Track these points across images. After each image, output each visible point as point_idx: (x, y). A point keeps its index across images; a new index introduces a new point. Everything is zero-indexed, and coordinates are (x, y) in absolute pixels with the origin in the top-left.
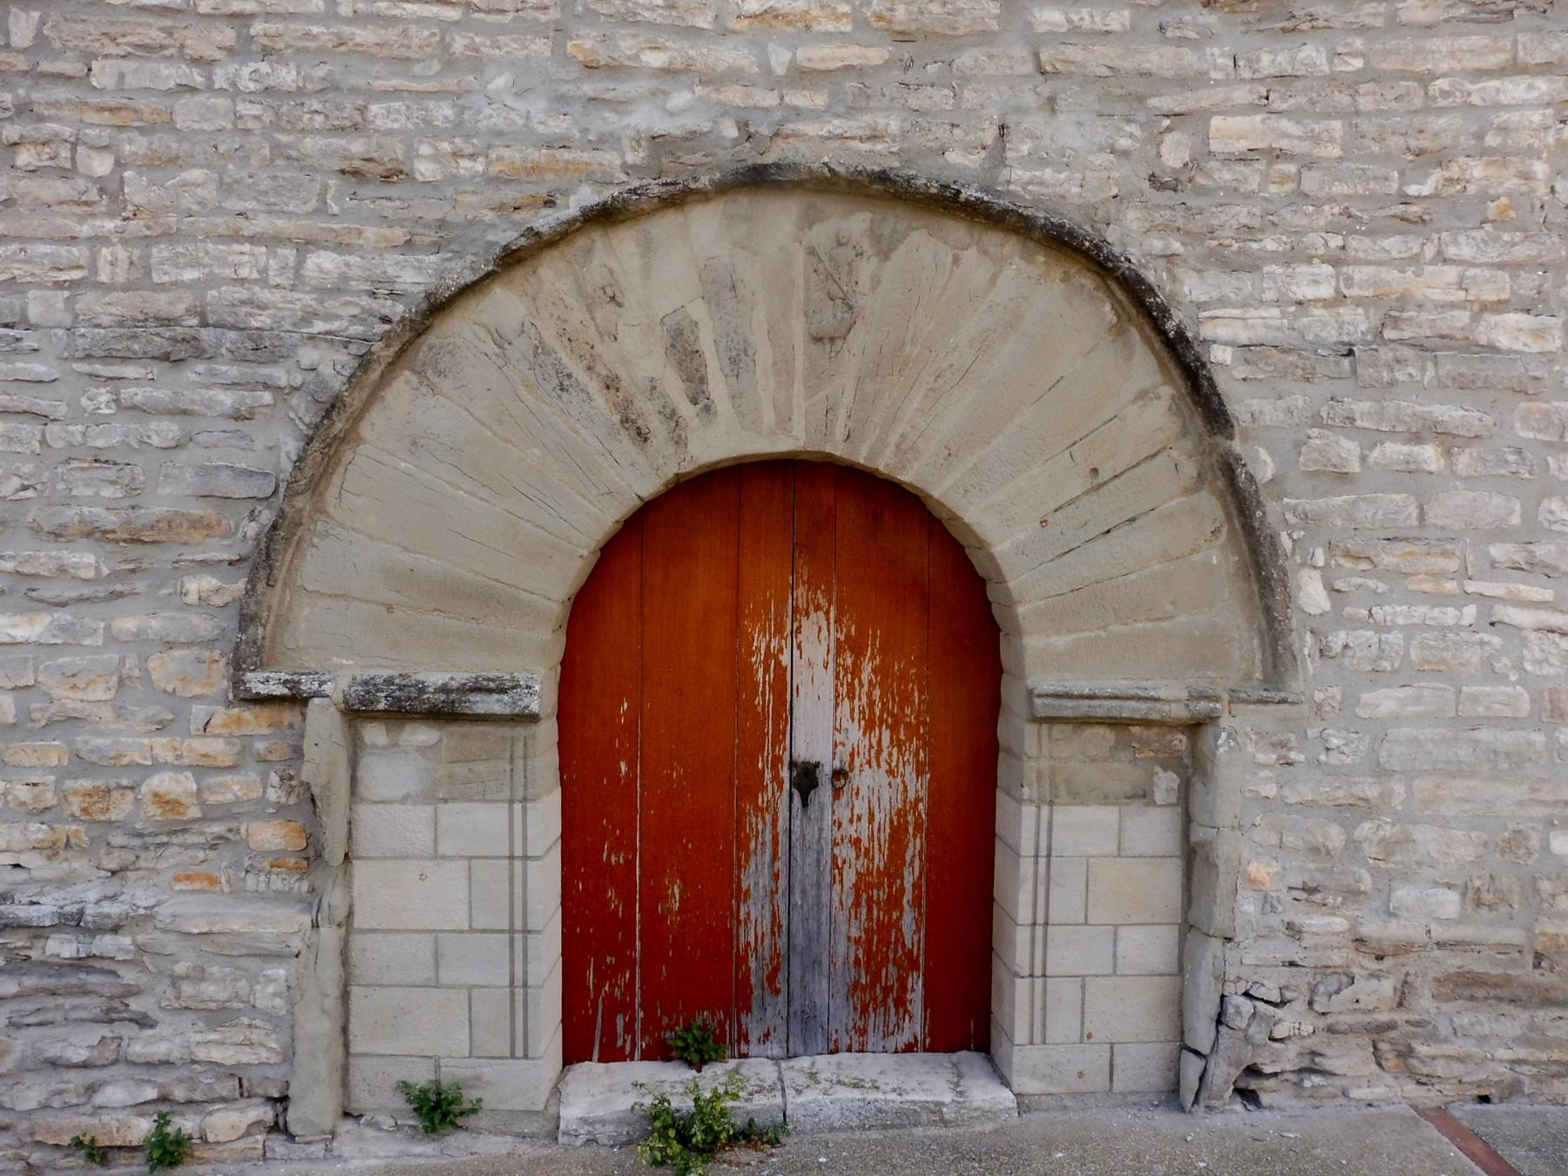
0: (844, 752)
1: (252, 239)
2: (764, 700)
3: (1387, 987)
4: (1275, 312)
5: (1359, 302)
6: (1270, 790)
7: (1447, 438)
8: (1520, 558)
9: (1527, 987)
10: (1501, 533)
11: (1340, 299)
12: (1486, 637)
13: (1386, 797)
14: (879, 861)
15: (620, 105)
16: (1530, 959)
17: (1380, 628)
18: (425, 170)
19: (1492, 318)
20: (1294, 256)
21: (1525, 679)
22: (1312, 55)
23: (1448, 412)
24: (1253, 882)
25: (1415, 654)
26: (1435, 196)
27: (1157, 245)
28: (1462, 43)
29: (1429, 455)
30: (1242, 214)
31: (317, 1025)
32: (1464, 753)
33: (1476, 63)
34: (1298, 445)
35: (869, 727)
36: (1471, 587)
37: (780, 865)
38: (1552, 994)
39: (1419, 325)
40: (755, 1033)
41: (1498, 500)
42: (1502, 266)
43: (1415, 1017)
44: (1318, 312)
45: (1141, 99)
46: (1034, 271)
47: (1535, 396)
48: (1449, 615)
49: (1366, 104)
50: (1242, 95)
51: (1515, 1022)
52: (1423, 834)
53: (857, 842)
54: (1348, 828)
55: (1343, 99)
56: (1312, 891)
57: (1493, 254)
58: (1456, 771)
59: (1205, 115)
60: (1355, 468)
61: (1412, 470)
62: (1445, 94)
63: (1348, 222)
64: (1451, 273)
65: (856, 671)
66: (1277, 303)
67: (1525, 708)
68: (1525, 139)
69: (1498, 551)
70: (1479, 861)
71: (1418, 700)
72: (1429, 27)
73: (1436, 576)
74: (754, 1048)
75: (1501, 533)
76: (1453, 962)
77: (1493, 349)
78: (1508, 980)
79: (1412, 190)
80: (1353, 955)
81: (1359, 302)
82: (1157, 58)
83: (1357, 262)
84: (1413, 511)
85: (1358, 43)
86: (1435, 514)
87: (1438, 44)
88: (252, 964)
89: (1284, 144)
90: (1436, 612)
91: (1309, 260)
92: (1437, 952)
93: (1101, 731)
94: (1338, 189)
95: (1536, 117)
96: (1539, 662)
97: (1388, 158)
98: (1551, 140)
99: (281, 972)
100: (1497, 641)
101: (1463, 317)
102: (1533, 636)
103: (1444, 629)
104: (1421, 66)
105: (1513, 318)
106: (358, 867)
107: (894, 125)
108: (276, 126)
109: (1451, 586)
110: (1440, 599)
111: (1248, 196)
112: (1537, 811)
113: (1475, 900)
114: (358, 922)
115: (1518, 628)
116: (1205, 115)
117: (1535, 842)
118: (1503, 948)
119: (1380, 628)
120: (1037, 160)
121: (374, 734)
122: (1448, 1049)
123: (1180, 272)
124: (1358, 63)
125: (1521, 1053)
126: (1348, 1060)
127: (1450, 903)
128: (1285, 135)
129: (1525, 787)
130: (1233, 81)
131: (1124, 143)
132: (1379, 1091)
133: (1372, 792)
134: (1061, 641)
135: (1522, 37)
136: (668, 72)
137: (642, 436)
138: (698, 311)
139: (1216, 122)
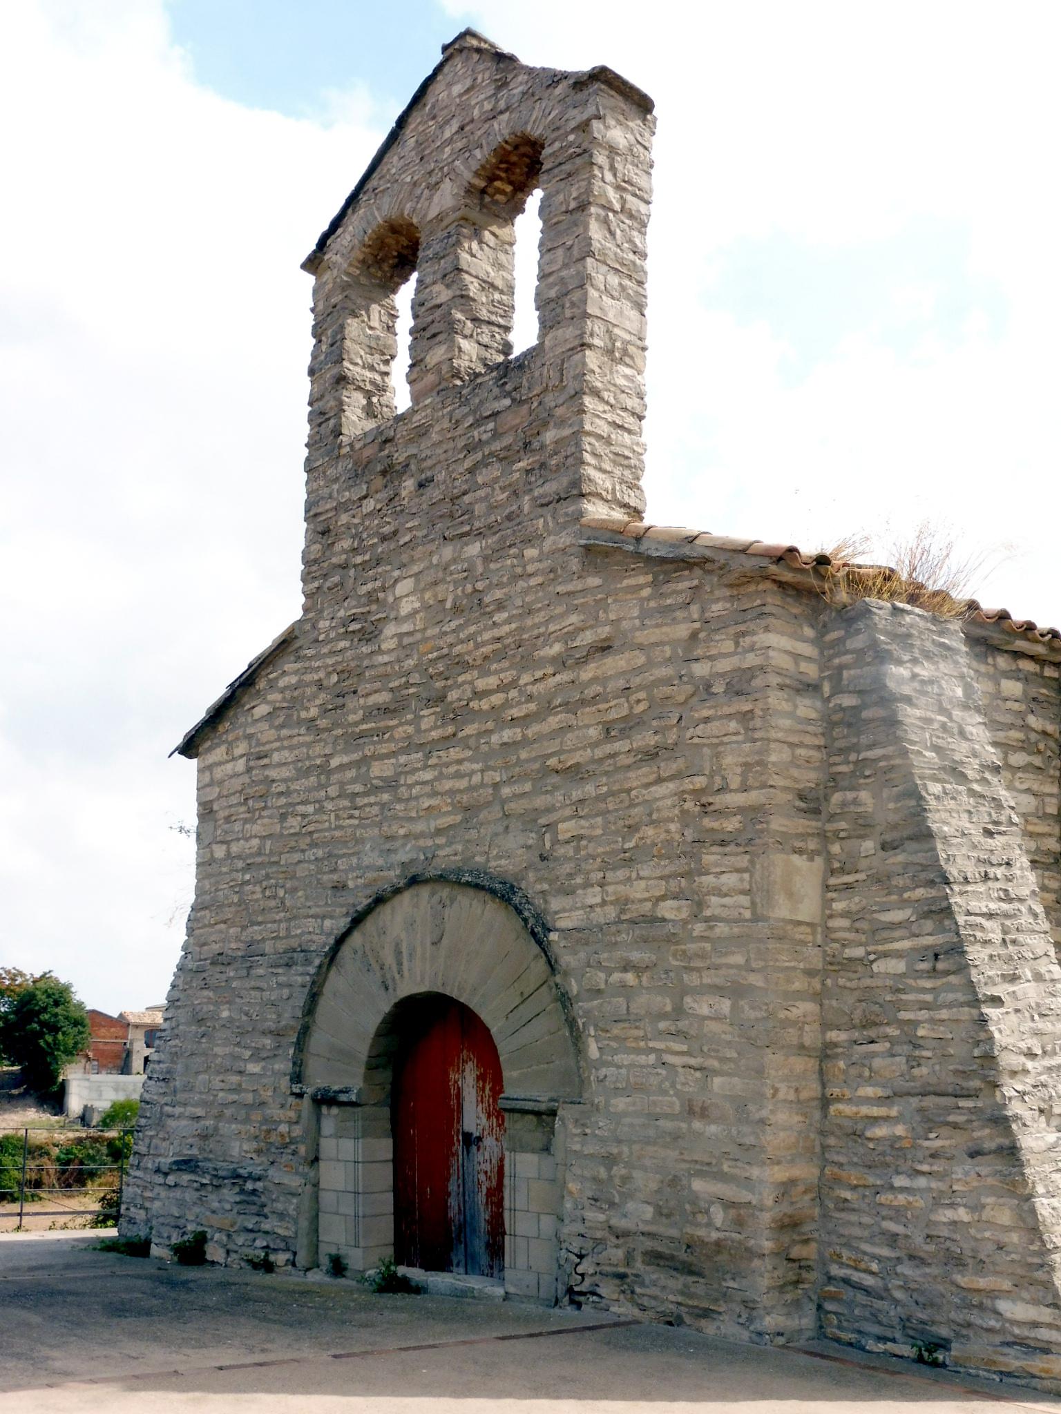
0: (480, 1128)
1: (312, 916)
2: (453, 1102)
3: (620, 1253)
4: (581, 912)
5: (612, 903)
6: (577, 1147)
7: (638, 969)
8: (673, 1029)
9: (683, 1263)
10: (663, 1016)
11: (604, 903)
12: (659, 1071)
13: (620, 1153)
14: (494, 1183)
15: (395, 851)
16: (684, 1247)
17: (619, 1067)
18: (351, 884)
19: (662, 904)
20: (587, 885)
21: (678, 1094)
22: (589, 789)
23: (636, 956)
24: (571, 1193)
25: (632, 1080)
26: (637, 846)
27: (538, 887)
28: (640, 772)
29: (630, 978)
30: (568, 868)
31: (304, 1224)
32: (651, 1132)
33: (646, 780)
34: (583, 976)
35: (489, 1117)
36: (651, 1044)
37: (460, 1181)
38: (693, 1268)
39: (633, 911)
40: (455, 1262)
41: (659, 998)
42: (661, 878)
43: (634, 1272)
44: (598, 909)
45: (535, 821)
46: (495, 906)
47: (677, 943)
48: (642, 1059)
49: (611, 807)
50: (568, 812)
51: (681, 1281)
52: (637, 1174)
53: (486, 1173)
54: (609, 1169)
55: (603, 806)
56: (596, 1200)
57: (658, 873)
58: (648, 1142)
59: (556, 823)
60: (602, 986)
61: (623, 986)
62: (637, 797)
63: (605, 867)
64: (643, 884)
65: (483, 1090)
66: (583, 908)
67: (677, 1108)
68: (666, 814)
69: (662, 1025)
70: (658, 1191)
71: (634, 1104)
72: (629, 766)
73: (636, 1039)
74: (455, 1269)
75: (663, 1016)
76: (649, 1244)
77: (664, 920)
78: (672, 1258)
79: (627, 846)
80: (607, 1235)
81: (612, 903)
82: (540, 801)
83: (610, 884)
84: (625, 1007)
85: (604, 780)
86: (633, 1006)
87: (632, 774)
88: (289, 1197)
89: (582, 832)
90: (638, 1058)
91: (592, 886)
92: (642, 1238)
93: (531, 1117)
94: (600, 850)
95: (669, 802)
96: (683, 1084)
97: (616, 832)
98: (676, 811)
99: (295, 1201)
100: (664, 1072)
101: (649, 905)
102: (680, 1070)
103: (642, 1067)
104: (627, 786)
105: (670, 903)
106: (322, 1164)
107: (459, 848)
108: (318, 873)
109: (642, 1044)
110: (638, 1051)
111: (570, 859)
112: (684, 1166)
113: (659, 1212)
114: (322, 1186)
115: (674, 1066)
116: (556, 823)
117: (685, 1182)
118: (672, 1239)
119: (619, 1067)
120: (499, 857)
121: (324, 1109)
122: (648, 1291)
123: (548, 898)
124: (605, 789)
125: (680, 1299)
126: (608, 1289)
127: (649, 1212)
128: (583, 828)
129: (677, 1152)
130: (564, 806)
131: (530, 842)
132: (622, 1310)
133: (615, 1151)
134: (515, 1074)
135: (662, 765)
136: (406, 836)
137: (387, 989)
138: (403, 935)
139: (560, 826)
